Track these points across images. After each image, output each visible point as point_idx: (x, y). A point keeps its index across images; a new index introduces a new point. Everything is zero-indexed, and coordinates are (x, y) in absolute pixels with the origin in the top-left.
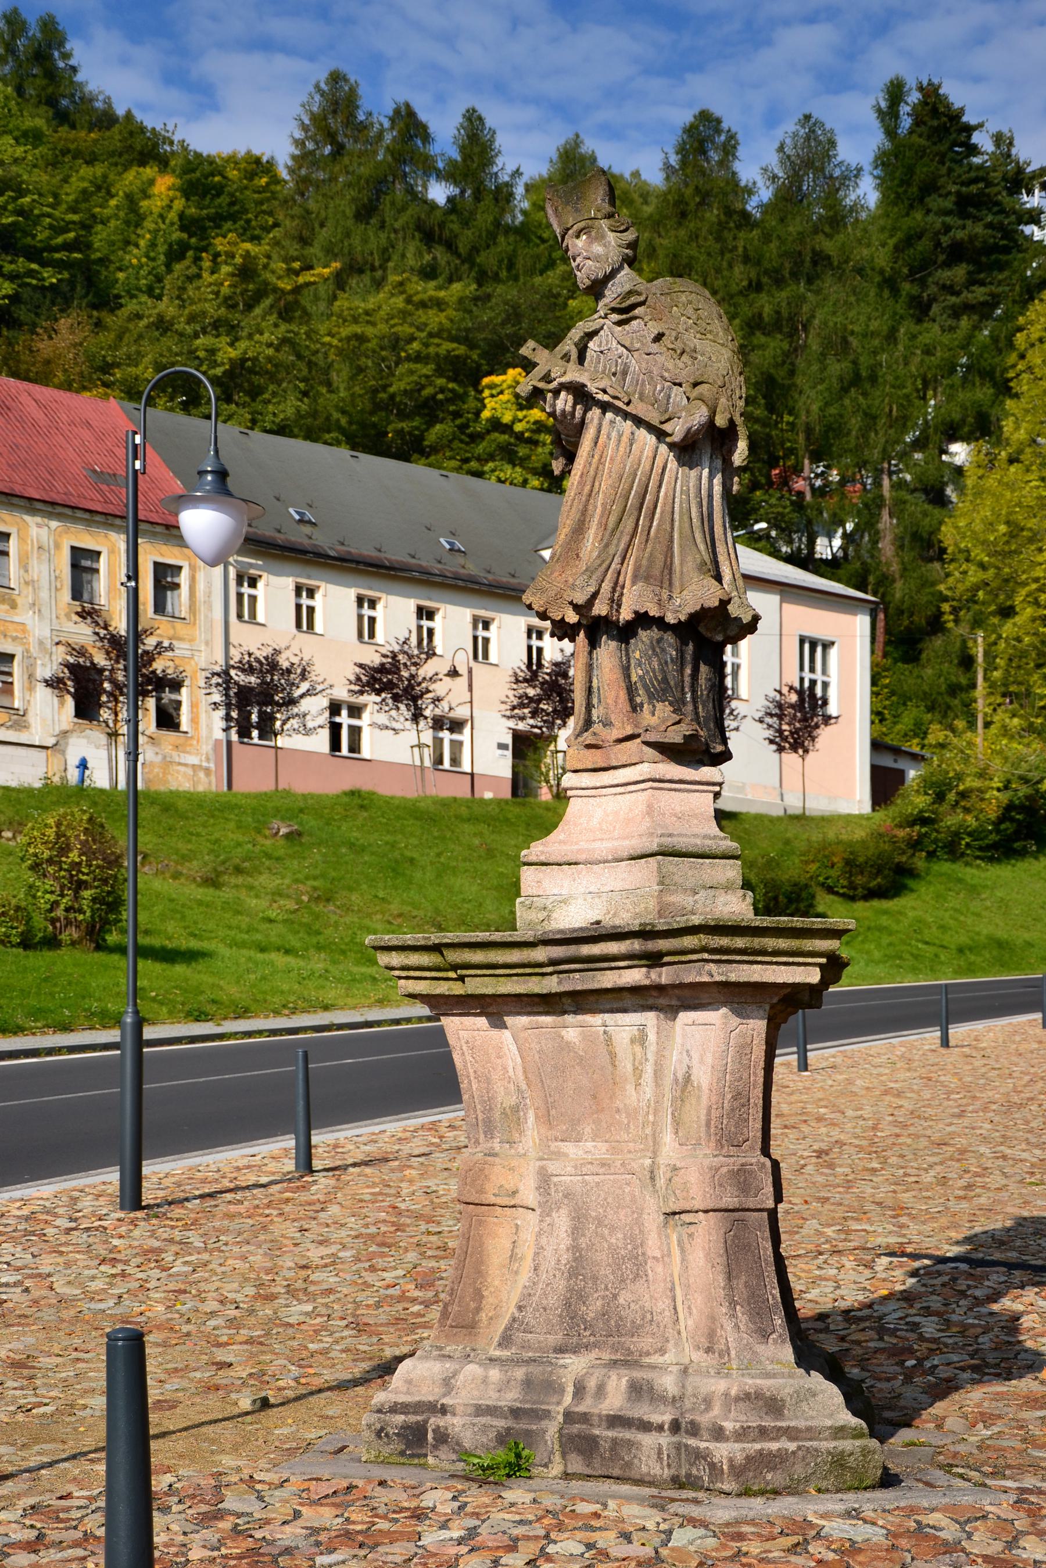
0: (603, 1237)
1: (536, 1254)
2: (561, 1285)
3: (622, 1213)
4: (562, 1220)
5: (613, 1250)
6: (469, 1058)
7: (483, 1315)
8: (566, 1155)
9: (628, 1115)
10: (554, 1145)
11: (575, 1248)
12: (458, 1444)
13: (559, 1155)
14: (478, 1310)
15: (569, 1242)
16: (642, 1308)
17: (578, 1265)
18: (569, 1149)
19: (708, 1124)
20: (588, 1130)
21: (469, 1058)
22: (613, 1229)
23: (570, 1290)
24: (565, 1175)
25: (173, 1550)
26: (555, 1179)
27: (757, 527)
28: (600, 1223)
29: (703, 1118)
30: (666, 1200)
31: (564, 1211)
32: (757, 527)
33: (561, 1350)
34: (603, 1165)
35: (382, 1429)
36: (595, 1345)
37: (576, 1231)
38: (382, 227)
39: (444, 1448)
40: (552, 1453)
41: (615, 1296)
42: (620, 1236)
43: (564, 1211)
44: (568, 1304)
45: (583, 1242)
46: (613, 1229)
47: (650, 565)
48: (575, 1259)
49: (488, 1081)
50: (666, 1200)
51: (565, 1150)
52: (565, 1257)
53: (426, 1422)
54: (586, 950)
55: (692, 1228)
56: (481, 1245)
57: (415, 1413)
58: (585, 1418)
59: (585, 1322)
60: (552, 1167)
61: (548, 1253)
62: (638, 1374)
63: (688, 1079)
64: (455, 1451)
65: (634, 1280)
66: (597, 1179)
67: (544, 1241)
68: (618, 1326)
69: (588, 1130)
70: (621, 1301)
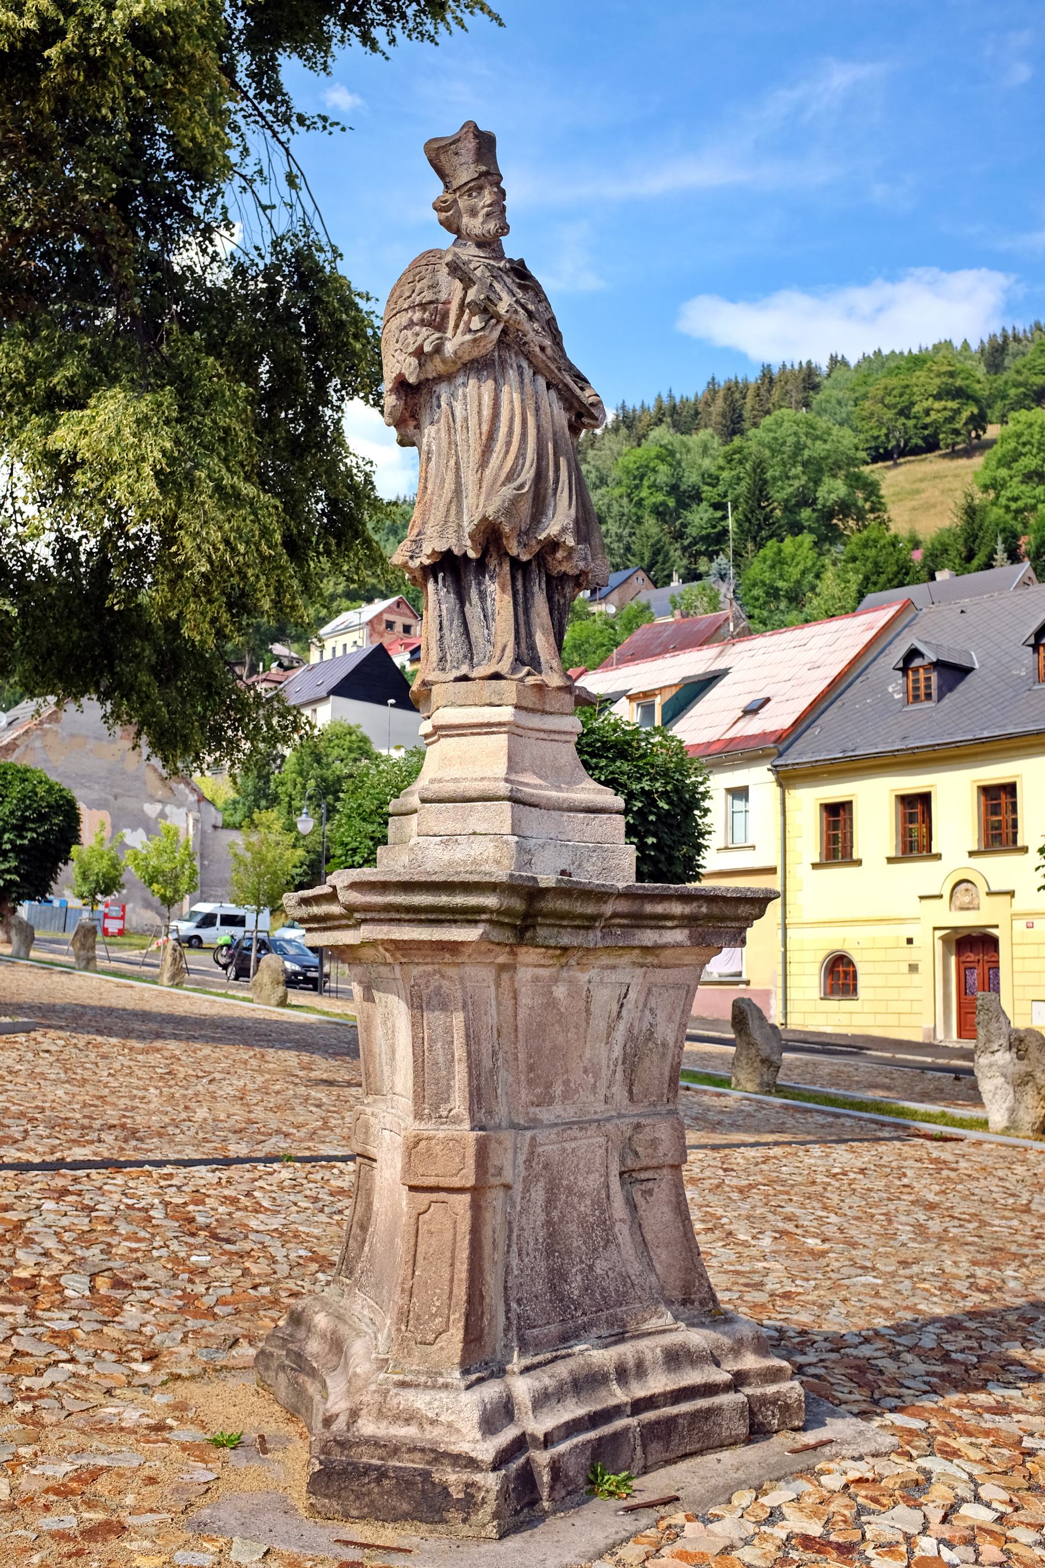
2: (542, 1266)
3: (591, 1177)
5: (582, 1220)
11: (549, 1223)
15: (542, 1217)
16: (620, 1274)
17: (553, 1243)
22: (582, 1196)
23: (551, 1270)
25: (935, 1299)
27: (666, 807)
28: (570, 1190)
29: (667, 1074)
32: (666, 807)
37: (550, 1203)
38: (155, 435)
41: (591, 1268)
42: (588, 1202)
44: (553, 1288)
46: (582, 1196)
47: (916, 689)
55: (650, 1185)
59: (573, 1302)
65: (605, 1248)
68: (604, 1298)
70: (599, 1271)
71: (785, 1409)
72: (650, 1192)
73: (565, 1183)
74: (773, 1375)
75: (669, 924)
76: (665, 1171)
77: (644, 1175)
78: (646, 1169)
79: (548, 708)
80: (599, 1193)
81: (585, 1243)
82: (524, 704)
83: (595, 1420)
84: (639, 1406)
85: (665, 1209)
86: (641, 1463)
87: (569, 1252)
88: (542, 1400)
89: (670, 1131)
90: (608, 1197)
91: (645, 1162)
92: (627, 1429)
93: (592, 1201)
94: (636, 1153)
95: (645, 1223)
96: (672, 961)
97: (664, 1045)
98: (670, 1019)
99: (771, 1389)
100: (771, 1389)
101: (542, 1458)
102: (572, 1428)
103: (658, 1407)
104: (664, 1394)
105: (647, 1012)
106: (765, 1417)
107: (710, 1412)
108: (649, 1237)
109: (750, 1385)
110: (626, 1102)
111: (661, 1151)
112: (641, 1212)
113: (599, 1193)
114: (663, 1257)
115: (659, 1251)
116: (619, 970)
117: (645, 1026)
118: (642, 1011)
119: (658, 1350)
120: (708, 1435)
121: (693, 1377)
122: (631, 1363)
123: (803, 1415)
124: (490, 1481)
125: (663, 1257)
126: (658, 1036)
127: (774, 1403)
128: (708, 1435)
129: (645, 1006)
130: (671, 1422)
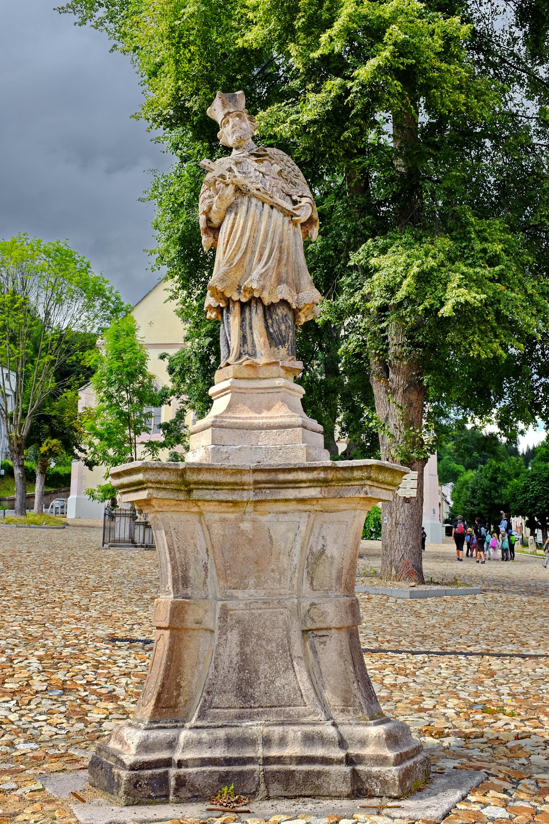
0: (261, 646)
1: (216, 658)
2: (234, 677)
4: (234, 637)
6: (175, 539)
7: (181, 699)
8: (237, 598)
9: (280, 574)
10: (229, 592)
11: (242, 654)
12: (192, 786)
13: (232, 597)
14: (178, 695)
15: (238, 650)
18: (239, 593)
19: (339, 578)
20: (252, 582)
21: (175, 539)
22: (269, 641)
24: (238, 608)
26: (231, 612)
28: (259, 637)
30: (304, 622)
31: (235, 632)
33: (240, 717)
34: (265, 603)
35: (138, 782)
36: (263, 713)
37: (243, 643)
39: (183, 789)
40: (259, 785)
41: (273, 682)
42: (274, 645)
43: (235, 632)
44: (239, 688)
45: (248, 650)
46: (269, 641)
48: (243, 660)
49: (185, 552)
50: (304, 622)
51: (236, 594)
52: (235, 659)
53: (166, 773)
54: (281, 477)
55: (324, 639)
56: (181, 655)
57: (156, 767)
58: (279, 760)
60: (230, 604)
61: (225, 657)
62: (309, 729)
63: (322, 552)
64: (190, 791)
65: (284, 671)
66: (260, 612)
67: (221, 650)
69: (252, 582)
71: (384, 783)
72: (324, 643)
73: (255, 632)
74: (382, 761)
75: (303, 485)
76: (333, 631)
77: (320, 633)
78: (322, 629)
79: (261, 376)
80: (282, 640)
81: (270, 667)
82: (240, 376)
83: (228, 761)
84: (267, 760)
85: (334, 654)
86: (265, 793)
87: (256, 672)
88: (188, 745)
89: (334, 608)
90: (289, 642)
91: (319, 625)
92: (253, 772)
93: (277, 645)
94: (313, 619)
95: (321, 662)
96: (332, 508)
97: (332, 557)
98: (335, 542)
99: (375, 769)
100: (375, 769)
101: (173, 771)
102: (204, 762)
103: (284, 764)
104: (291, 757)
105: (321, 538)
106: (371, 786)
107: (319, 774)
108: (323, 670)
109: (366, 764)
110: (309, 590)
111: (329, 619)
112: (319, 655)
113: (282, 640)
114: (332, 682)
115: (329, 678)
116: (290, 514)
117: (320, 547)
118: (318, 538)
119: (299, 733)
120: (318, 787)
121: (319, 752)
122: (276, 737)
123: (397, 789)
124: (125, 774)
125: (332, 682)
126: (328, 552)
127: (377, 778)
128: (318, 787)
129: (319, 534)
130: (292, 773)
